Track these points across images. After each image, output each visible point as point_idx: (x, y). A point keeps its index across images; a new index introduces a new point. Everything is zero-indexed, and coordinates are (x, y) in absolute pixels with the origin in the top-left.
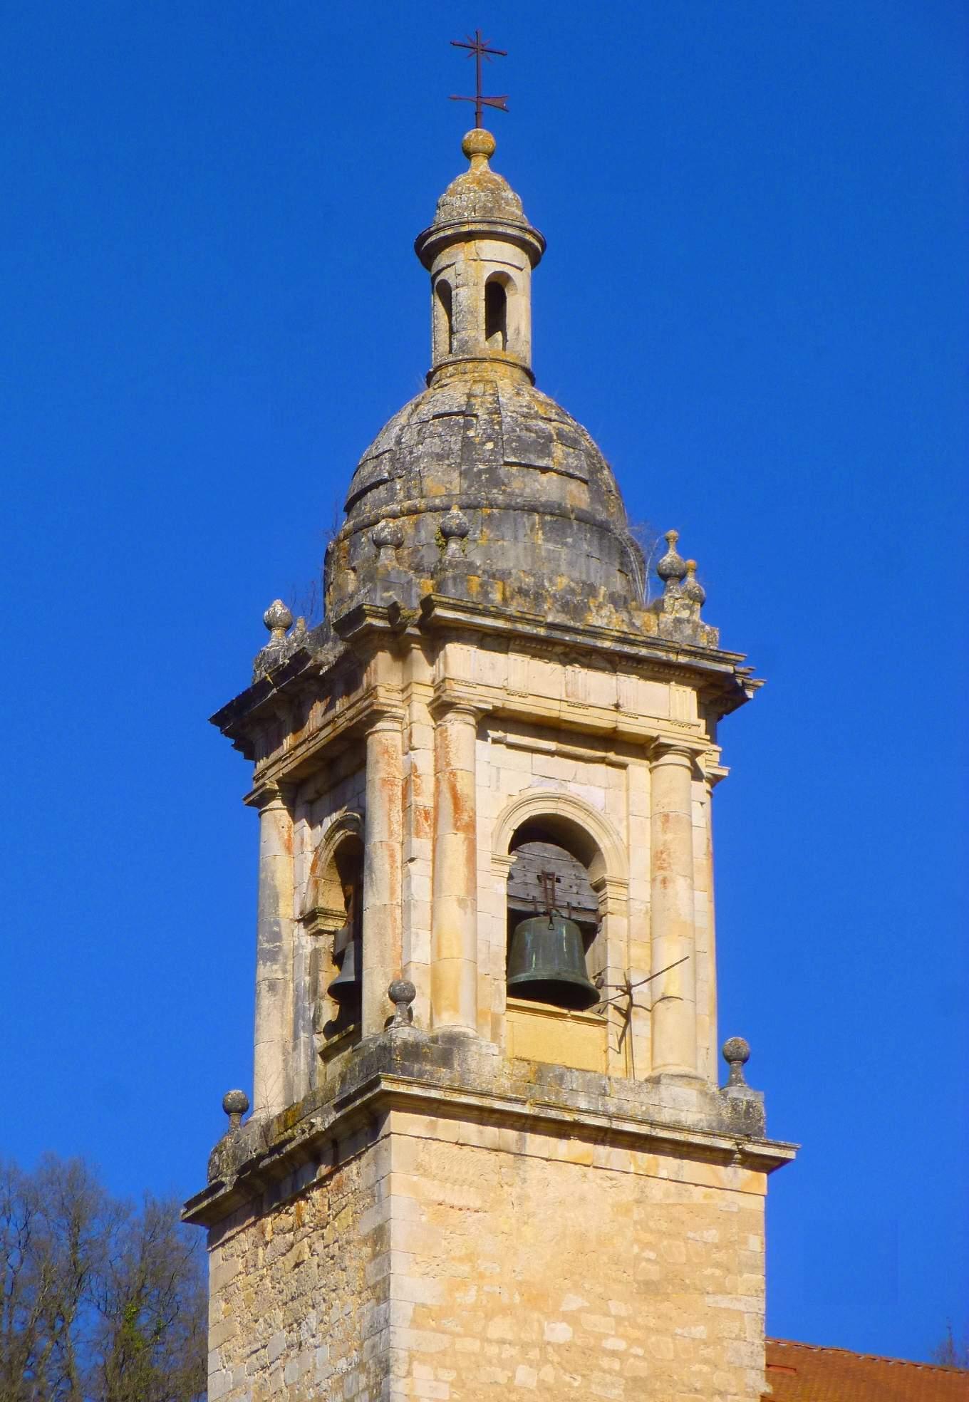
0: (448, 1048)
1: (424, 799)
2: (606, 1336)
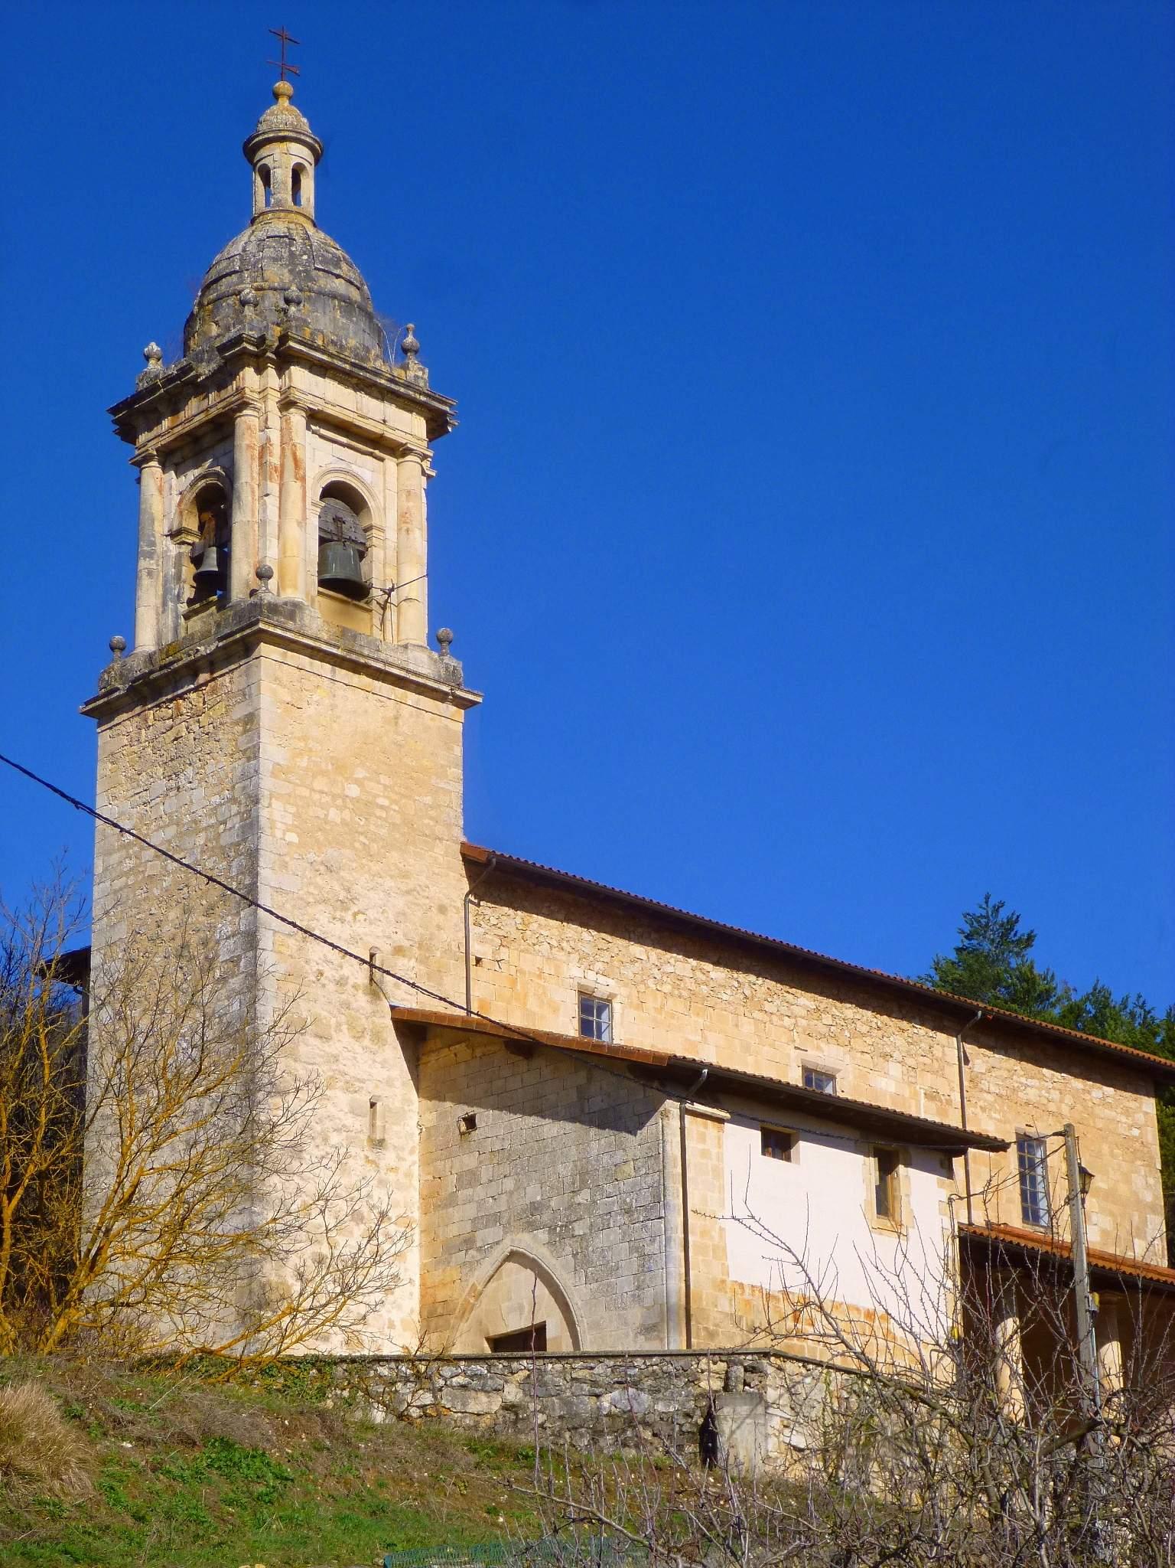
0: (293, 610)
1: (274, 459)
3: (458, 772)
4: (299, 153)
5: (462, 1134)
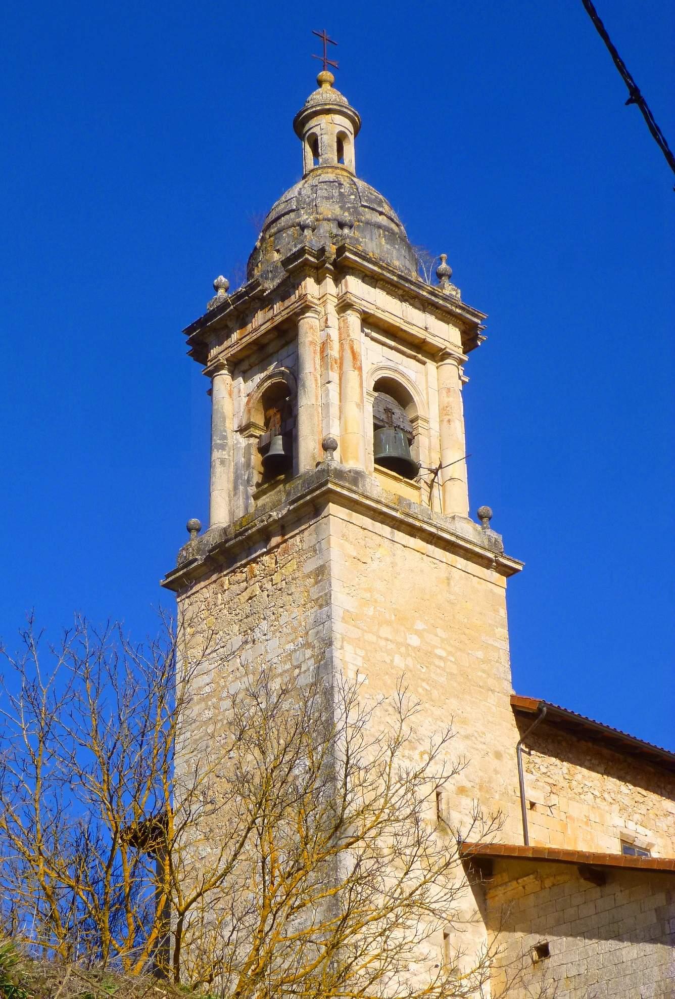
0: (356, 477)
2: (437, 647)
3: (504, 632)
4: (343, 123)
5: (534, 962)
